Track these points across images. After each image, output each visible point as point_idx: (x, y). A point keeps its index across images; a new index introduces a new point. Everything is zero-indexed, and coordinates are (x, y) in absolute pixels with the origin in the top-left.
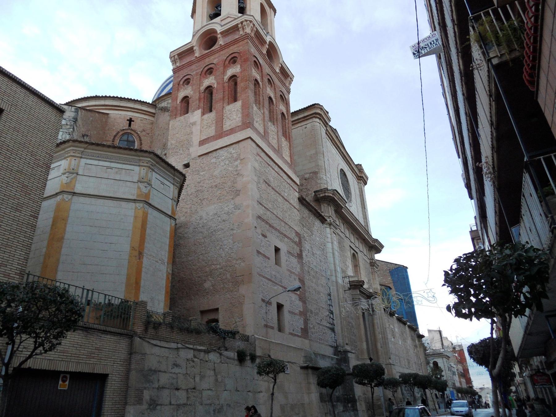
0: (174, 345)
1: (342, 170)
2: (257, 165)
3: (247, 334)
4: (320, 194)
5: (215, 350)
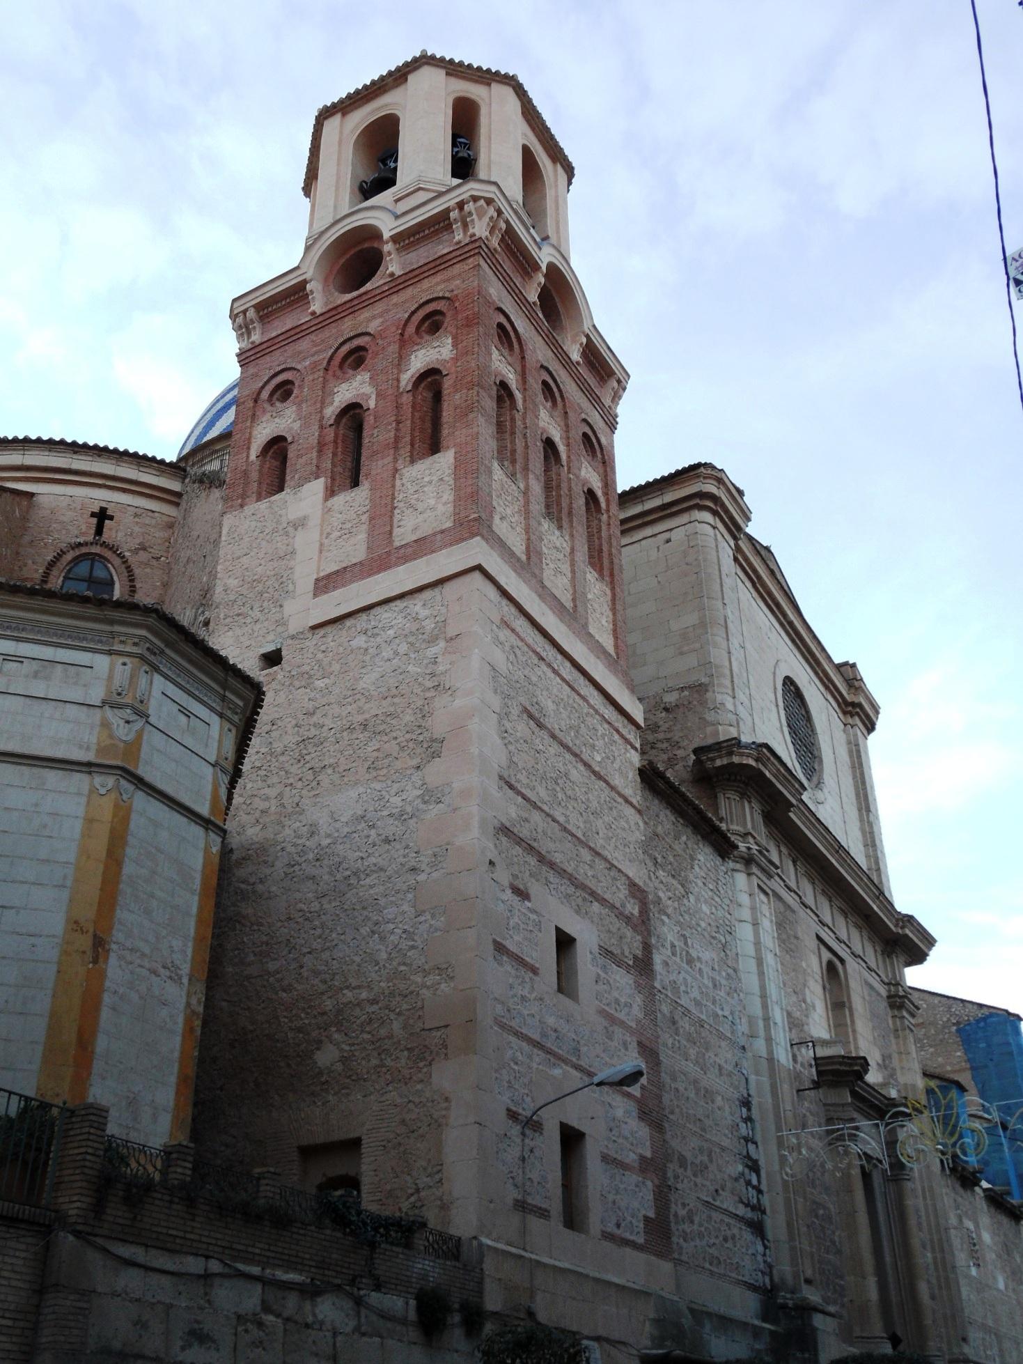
0: (194, 1265)
1: (789, 682)
2: (499, 657)
3: (453, 1231)
4: (713, 760)
5: (339, 1287)
